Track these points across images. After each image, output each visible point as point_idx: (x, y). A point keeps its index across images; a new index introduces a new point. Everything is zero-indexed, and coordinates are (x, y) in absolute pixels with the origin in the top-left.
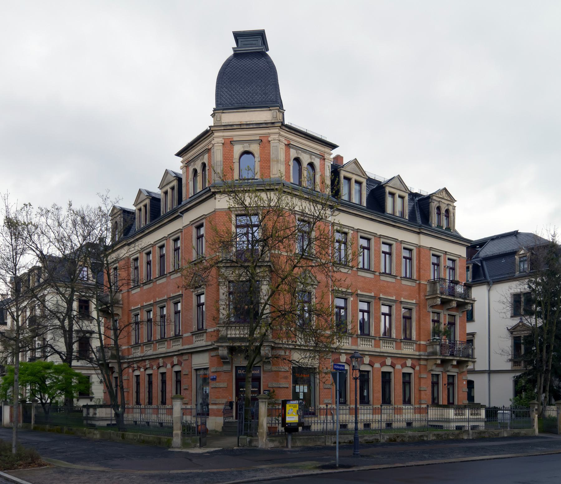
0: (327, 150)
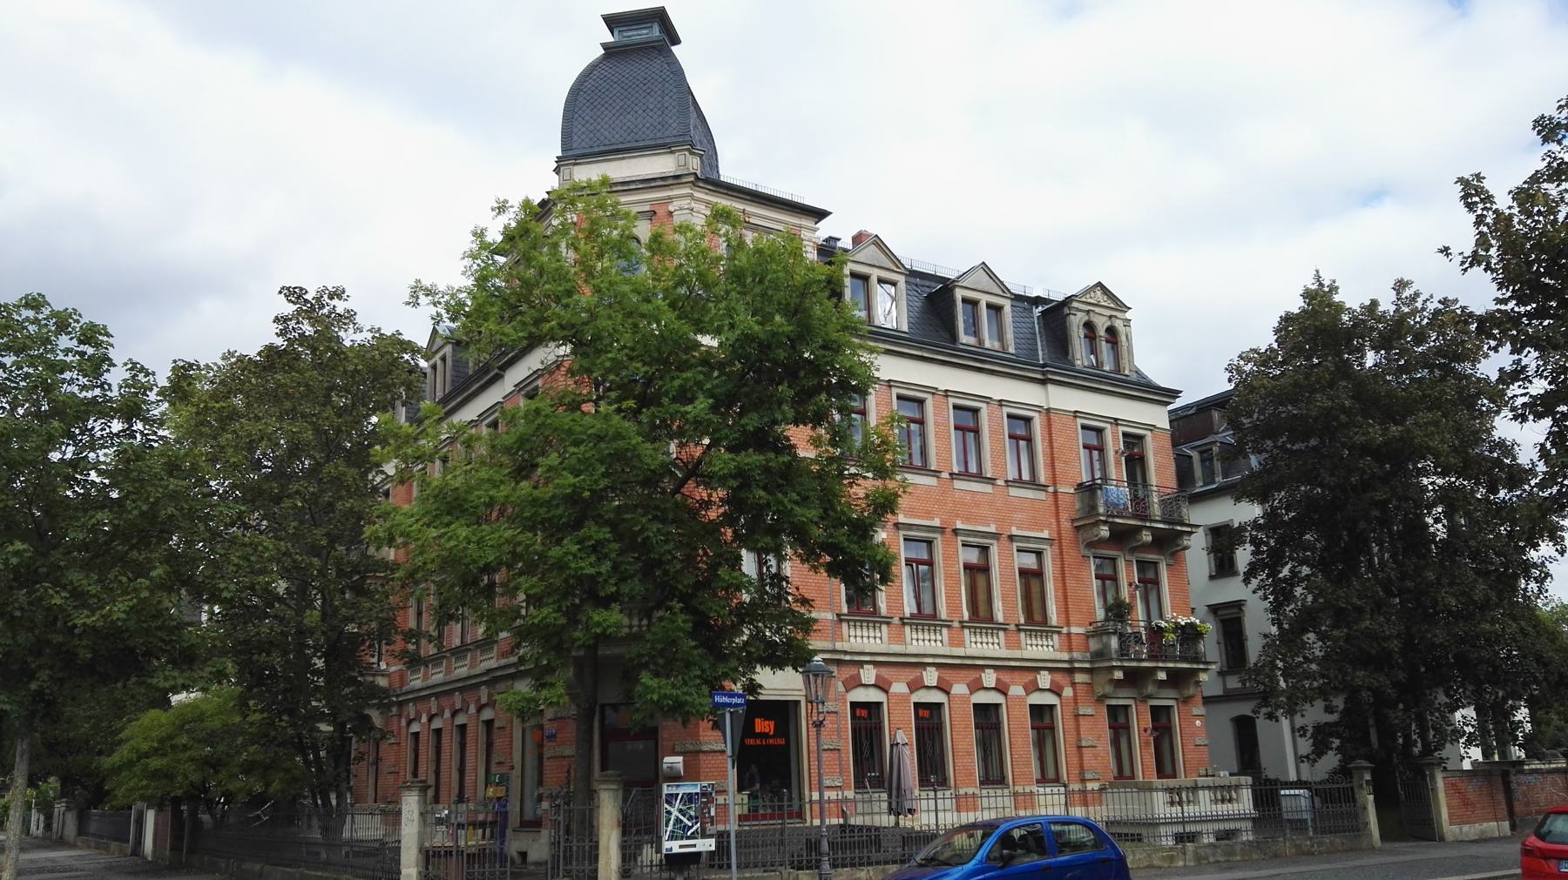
0: (806, 222)
